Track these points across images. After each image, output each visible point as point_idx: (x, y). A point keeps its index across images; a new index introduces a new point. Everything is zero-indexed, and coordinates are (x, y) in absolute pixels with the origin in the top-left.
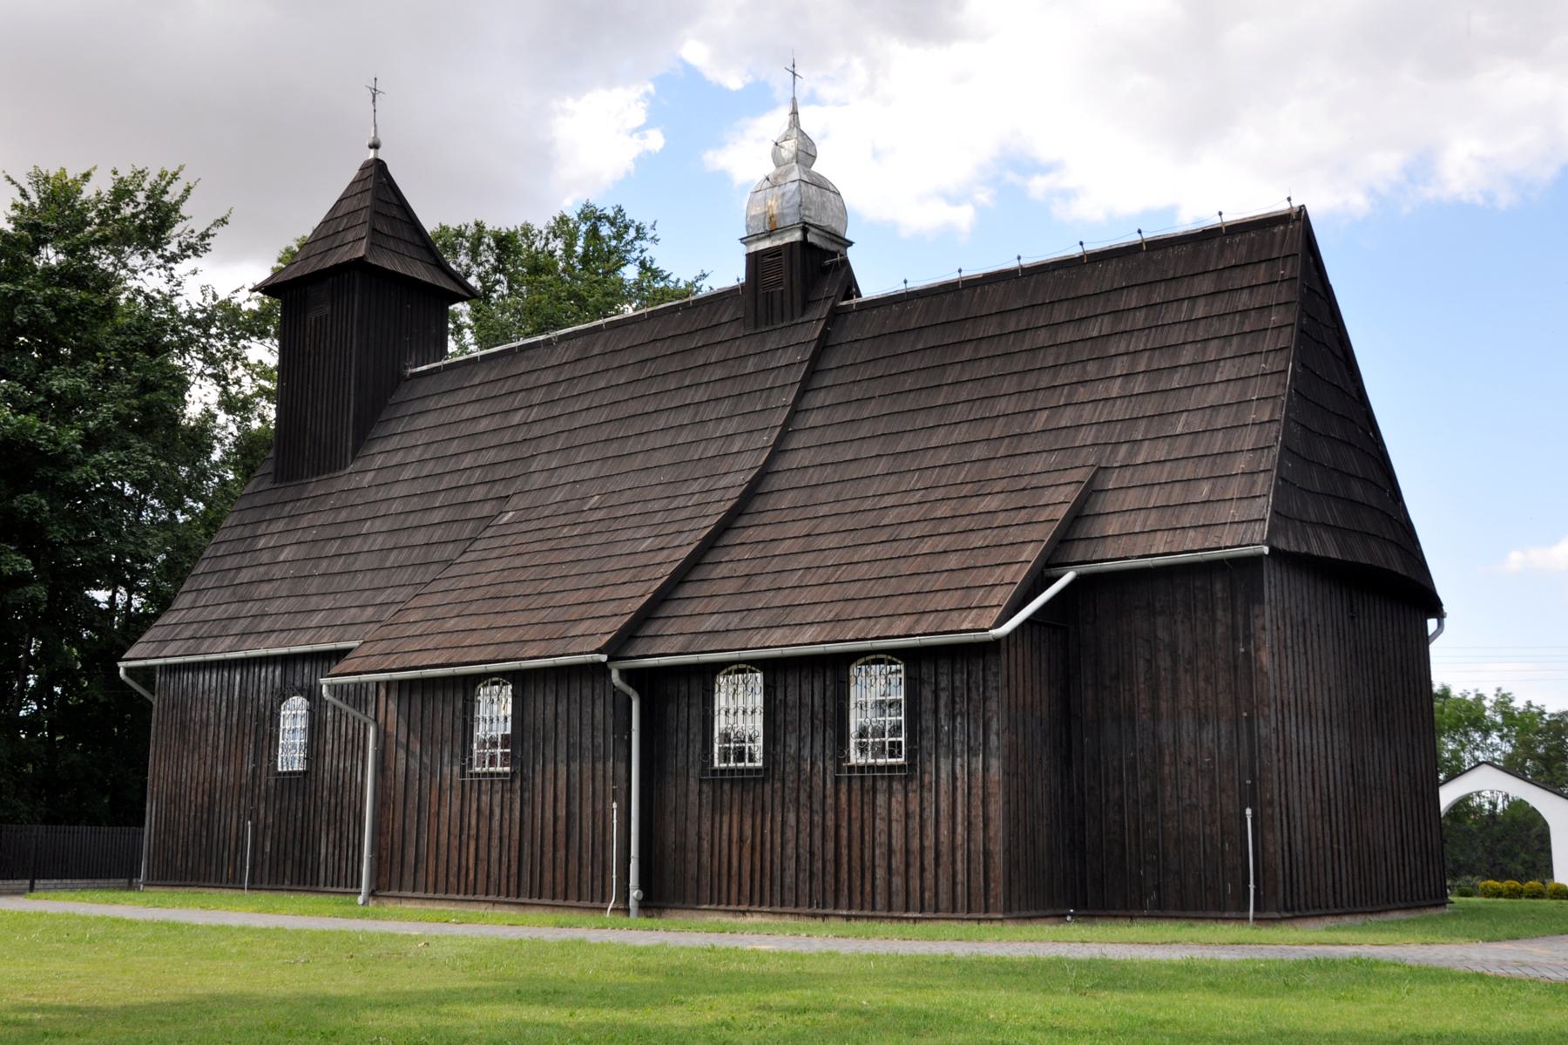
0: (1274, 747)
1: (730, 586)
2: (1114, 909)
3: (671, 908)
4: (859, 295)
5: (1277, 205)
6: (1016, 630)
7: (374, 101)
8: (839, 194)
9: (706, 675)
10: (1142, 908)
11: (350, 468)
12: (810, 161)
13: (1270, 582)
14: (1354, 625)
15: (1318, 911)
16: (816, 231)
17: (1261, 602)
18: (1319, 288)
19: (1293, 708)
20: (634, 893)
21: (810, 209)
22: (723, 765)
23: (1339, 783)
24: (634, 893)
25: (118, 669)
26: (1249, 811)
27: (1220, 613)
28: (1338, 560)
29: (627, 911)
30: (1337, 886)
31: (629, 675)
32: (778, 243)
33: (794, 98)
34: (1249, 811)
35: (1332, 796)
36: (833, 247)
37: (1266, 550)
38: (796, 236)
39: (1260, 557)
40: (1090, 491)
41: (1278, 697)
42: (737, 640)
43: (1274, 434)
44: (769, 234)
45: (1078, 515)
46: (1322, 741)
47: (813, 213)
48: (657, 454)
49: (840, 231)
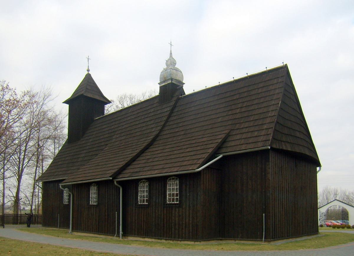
0: (271, 199)
1: (144, 161)
2: (231, 238)
3: (130, 236)
4: (185, 94)
5: (281, 65)
6: (203, 169)
7: (88, 61)
8: (181, 72)
9: (136, 183)
10: (238, 238)
11: (81, 140)
12: (175, 65)
13: (272, 156)
14: (296, 168)
15: (282, 238)
16: (175, 80)
17: (269, 161)
18: (290, 84)
19: (277, 189)
20: (121, 232)
21: (173, 75)
22: (169, 203)
23: (290, 207)
24: (121, 232)
25: (59, 186)
26: (264, 215)
27: (259, 165)
28: (290, 151)
29: (119, 236)
30: (288, 231)
31: (119, 183)
32: (166, 83)
33: (171, 51)
34: (264, 215)
35: (288, 210)
36: (179, 84)
37: (269, 147)
38: (170, 82)
39: (268, 149)
40: (228, 136)
41: (273, 186)
42: (141, 174)
43: (274, 119)
44: (164, 82)
45: (224, 141)
46: (286, 196)
47: (174, 76)
48: (137, 133)
49: (181, 80)
